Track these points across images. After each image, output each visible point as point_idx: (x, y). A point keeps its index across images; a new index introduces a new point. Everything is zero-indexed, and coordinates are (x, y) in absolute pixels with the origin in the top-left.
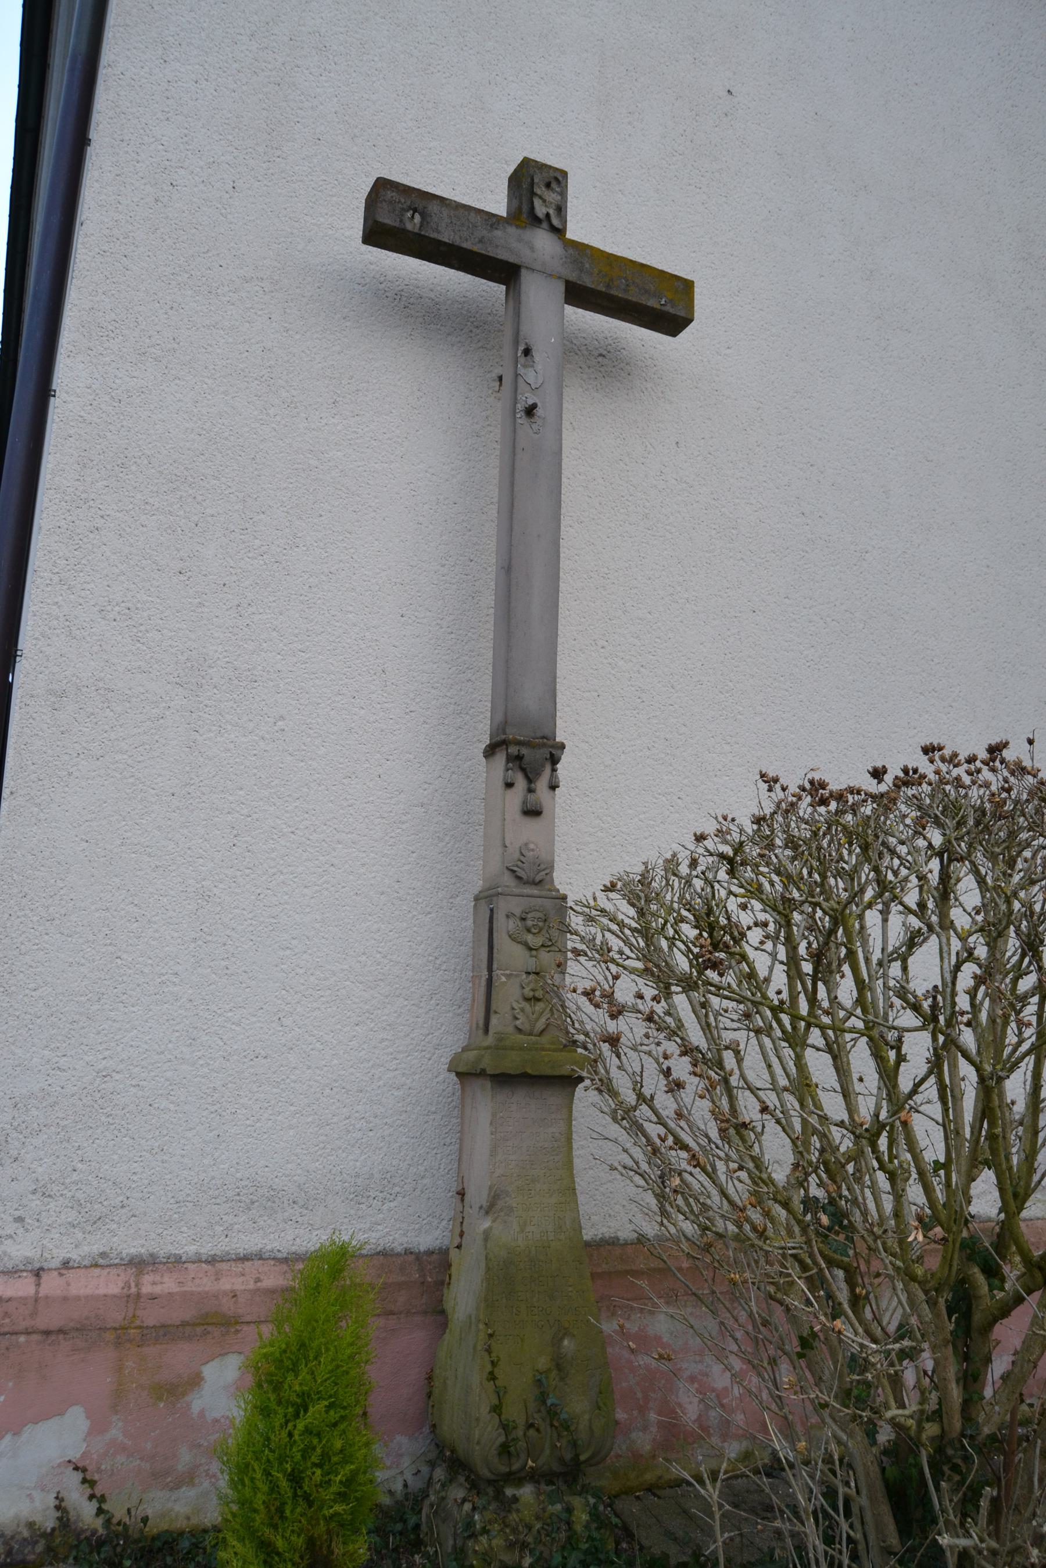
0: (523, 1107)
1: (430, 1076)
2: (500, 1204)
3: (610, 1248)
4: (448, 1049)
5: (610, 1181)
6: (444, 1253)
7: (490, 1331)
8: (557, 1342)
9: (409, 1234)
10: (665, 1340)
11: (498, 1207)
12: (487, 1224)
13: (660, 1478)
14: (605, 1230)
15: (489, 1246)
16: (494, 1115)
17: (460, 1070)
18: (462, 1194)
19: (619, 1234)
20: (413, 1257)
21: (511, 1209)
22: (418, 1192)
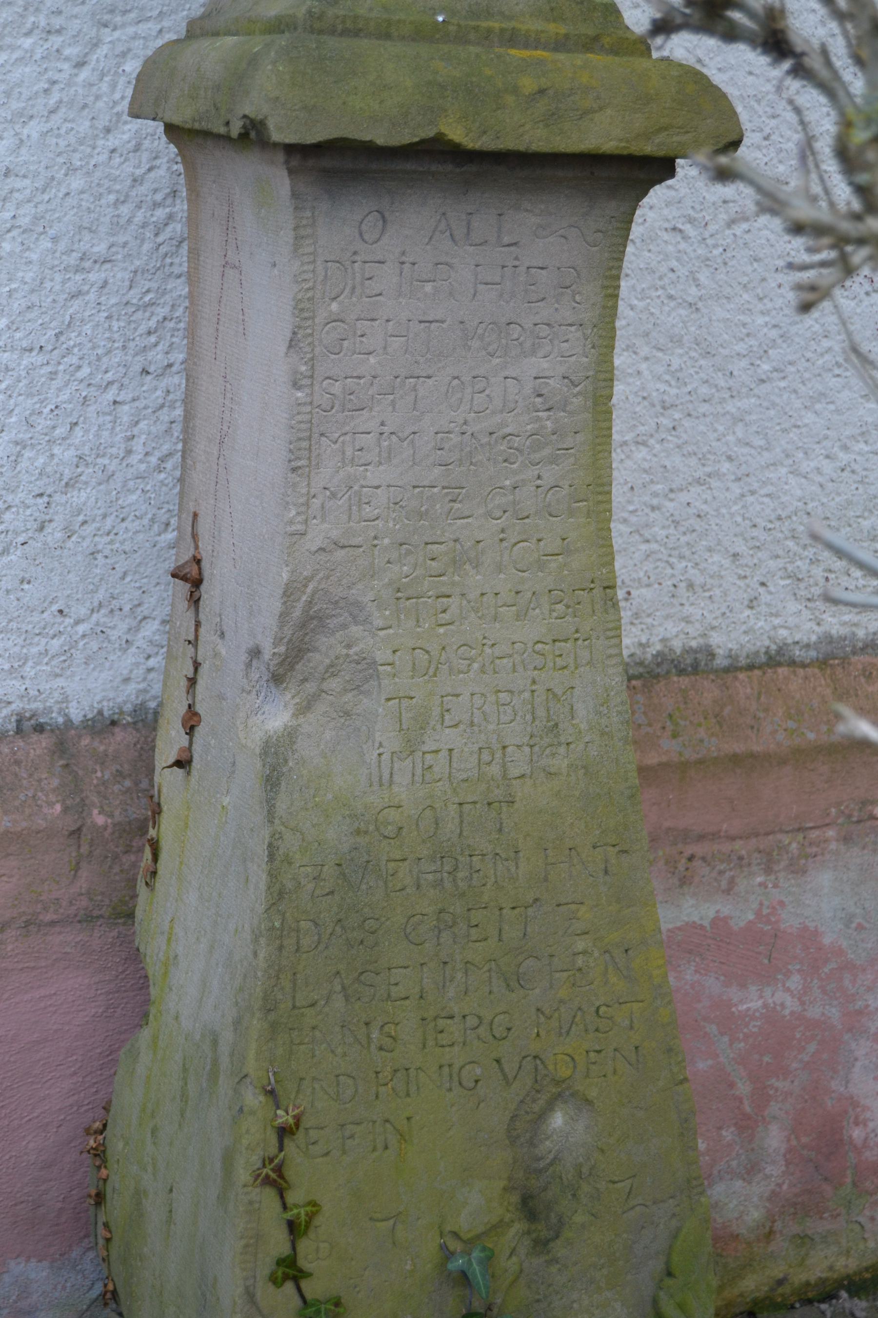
0: (421, 266)
1: (84, 126)
2: (328, 647)
3: (684, 682)
4: (152, 27)
5: (698, 482)
6: (145, 721)
7: (284, 1118)
8: (524, 1127)
9: (29, 670)
10: (827, 940)
11: (318, 660)
12: (276, 717)
13: (780, 1282)
14: (671, 629)
15: (281, 806)
16: (303, 310)
17: (176, 120)
18: (191, 578)
19: (716, 639)
20: (45, 741)
21: (367, 670)
22: (54, 534)
